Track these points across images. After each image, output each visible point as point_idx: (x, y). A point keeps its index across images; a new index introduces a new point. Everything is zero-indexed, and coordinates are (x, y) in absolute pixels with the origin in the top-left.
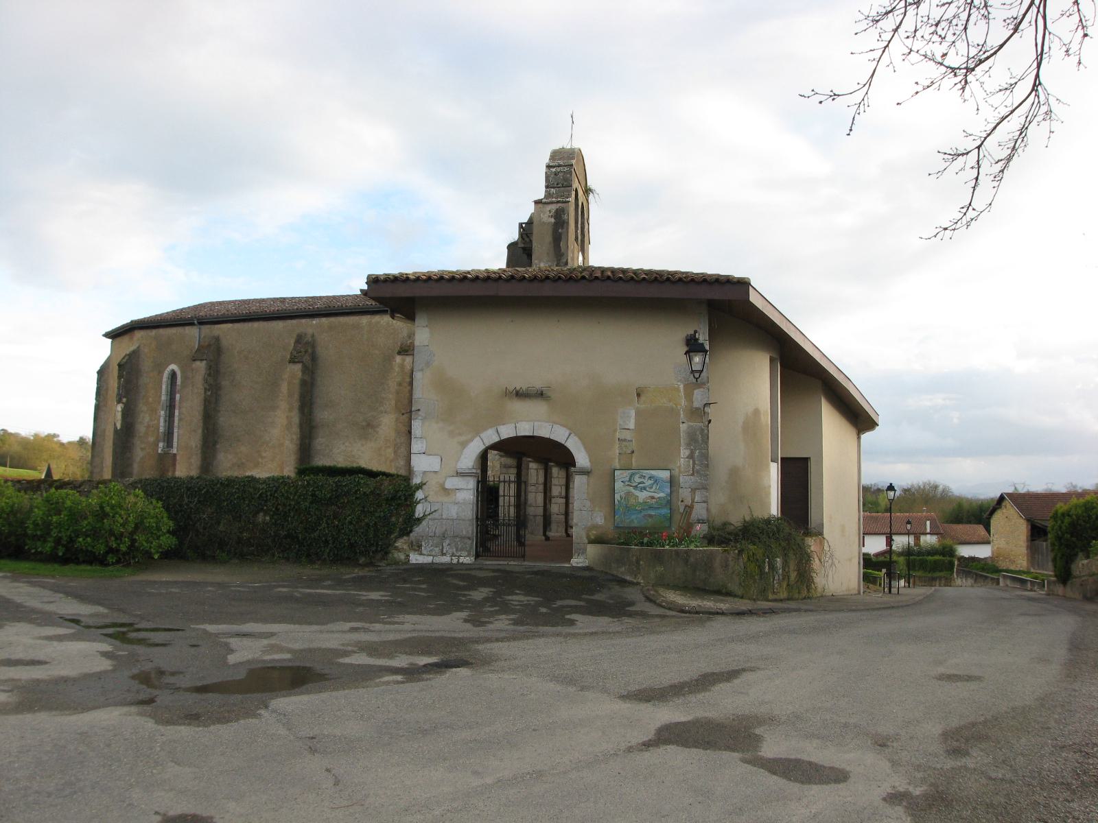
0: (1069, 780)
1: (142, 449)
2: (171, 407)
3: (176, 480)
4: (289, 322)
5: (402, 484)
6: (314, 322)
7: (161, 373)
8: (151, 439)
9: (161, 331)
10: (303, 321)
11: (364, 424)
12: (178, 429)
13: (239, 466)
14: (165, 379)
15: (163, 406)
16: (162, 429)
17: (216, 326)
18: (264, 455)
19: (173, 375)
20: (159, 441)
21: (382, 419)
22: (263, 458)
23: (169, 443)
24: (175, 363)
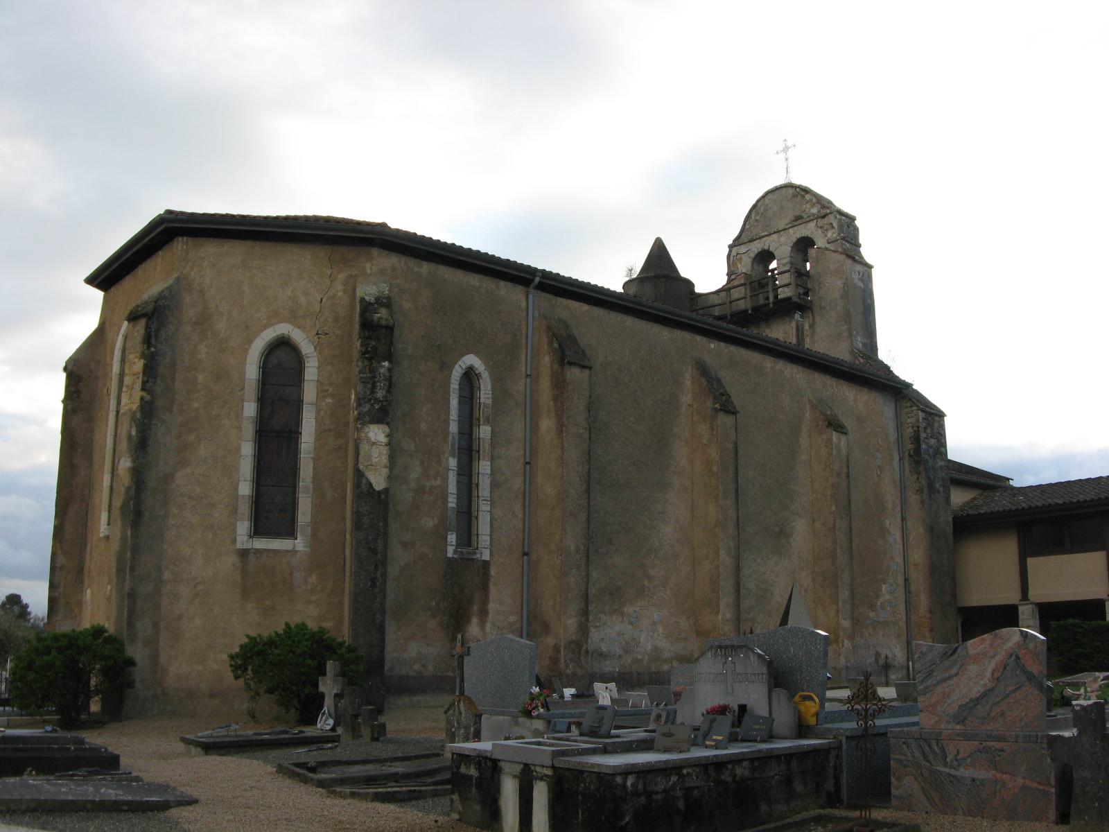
0: (824, 447)
1: (405, 545)
2: (468, 452)
3: (86, 629)
4: (678, 334)
5: (901, 615)
6: (712, 346)
7: (446, 367)
8: (429, 523)
9: (446, 272)
10: (698, 338)
11: (776, 529)
12: (492, 506)
13: (611, 594)
14: (454, 386)
15: (453, 445)
16: (452, 502)
17: (560, 300)
18: (652, 573)
19: (470, 376)
20: (447, 529)
21: (794, 524)
22: (650, 578)
23: (467, 537)
24: (478, 354)
